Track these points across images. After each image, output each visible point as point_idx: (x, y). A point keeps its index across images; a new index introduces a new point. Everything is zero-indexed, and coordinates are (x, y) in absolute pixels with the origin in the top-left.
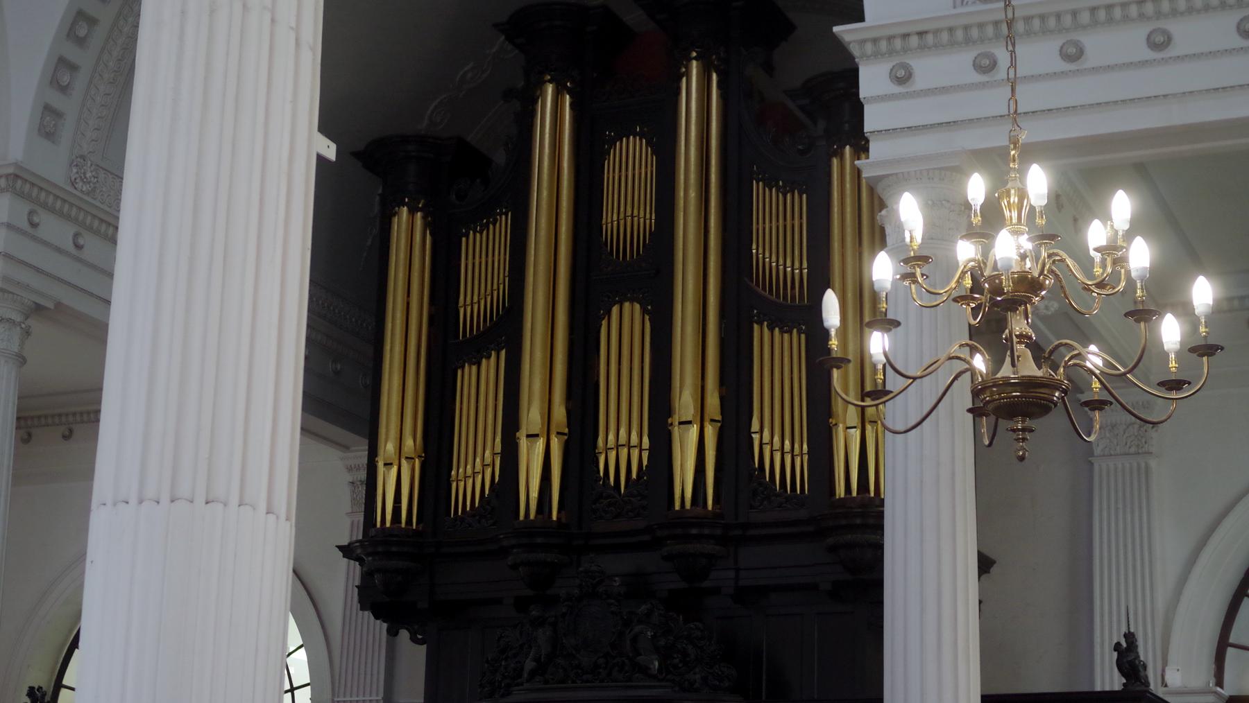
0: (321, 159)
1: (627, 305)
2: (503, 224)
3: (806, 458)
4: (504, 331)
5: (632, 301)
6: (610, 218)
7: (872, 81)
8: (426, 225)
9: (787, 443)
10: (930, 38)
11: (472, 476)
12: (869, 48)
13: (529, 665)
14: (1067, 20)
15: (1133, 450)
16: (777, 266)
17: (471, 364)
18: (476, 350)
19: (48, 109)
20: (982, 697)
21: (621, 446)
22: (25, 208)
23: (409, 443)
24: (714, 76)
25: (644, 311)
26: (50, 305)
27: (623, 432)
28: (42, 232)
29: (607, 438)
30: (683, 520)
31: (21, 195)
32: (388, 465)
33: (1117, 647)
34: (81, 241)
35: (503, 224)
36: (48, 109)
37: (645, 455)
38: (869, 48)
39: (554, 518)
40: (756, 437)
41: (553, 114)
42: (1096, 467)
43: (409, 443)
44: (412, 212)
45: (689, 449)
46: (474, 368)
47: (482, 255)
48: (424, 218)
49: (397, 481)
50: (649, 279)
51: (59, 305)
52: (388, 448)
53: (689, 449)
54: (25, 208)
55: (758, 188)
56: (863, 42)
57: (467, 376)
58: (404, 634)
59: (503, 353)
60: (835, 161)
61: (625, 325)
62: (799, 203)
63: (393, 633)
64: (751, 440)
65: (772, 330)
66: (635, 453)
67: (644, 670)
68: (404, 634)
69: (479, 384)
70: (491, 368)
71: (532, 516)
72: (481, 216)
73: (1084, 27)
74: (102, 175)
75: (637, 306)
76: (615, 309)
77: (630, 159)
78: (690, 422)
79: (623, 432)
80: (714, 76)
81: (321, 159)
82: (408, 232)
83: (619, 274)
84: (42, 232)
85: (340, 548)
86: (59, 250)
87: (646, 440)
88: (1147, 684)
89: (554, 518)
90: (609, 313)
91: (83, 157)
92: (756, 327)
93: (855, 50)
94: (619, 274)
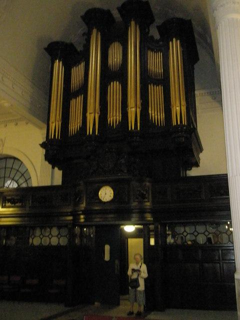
1: (115, 82)
2: (82, 65)
3: (139, 111)
6: (110, 62)
11: (74, 125)
16: (160, 114)
17: (74, 98)
18: (75, 95)
20: (235, 309)
21: (114, 117)
30: (132, 131)
32: (52, 123)
35: (82, 65)
37: (120, 118)
43: (58, 117)
45: (133, 111)
53: (133, 111)
57: (73, 102)
58: (56, 169)
60: (171, 43)
61: (115, 87)
62: (160, 54)
63: (53, 168)
68: (56, 169)
69: (76, 104)
71: (91, 133)
72: (77, 63)
75: (118, 82)
76: (112, 83)
82: (58, 67)
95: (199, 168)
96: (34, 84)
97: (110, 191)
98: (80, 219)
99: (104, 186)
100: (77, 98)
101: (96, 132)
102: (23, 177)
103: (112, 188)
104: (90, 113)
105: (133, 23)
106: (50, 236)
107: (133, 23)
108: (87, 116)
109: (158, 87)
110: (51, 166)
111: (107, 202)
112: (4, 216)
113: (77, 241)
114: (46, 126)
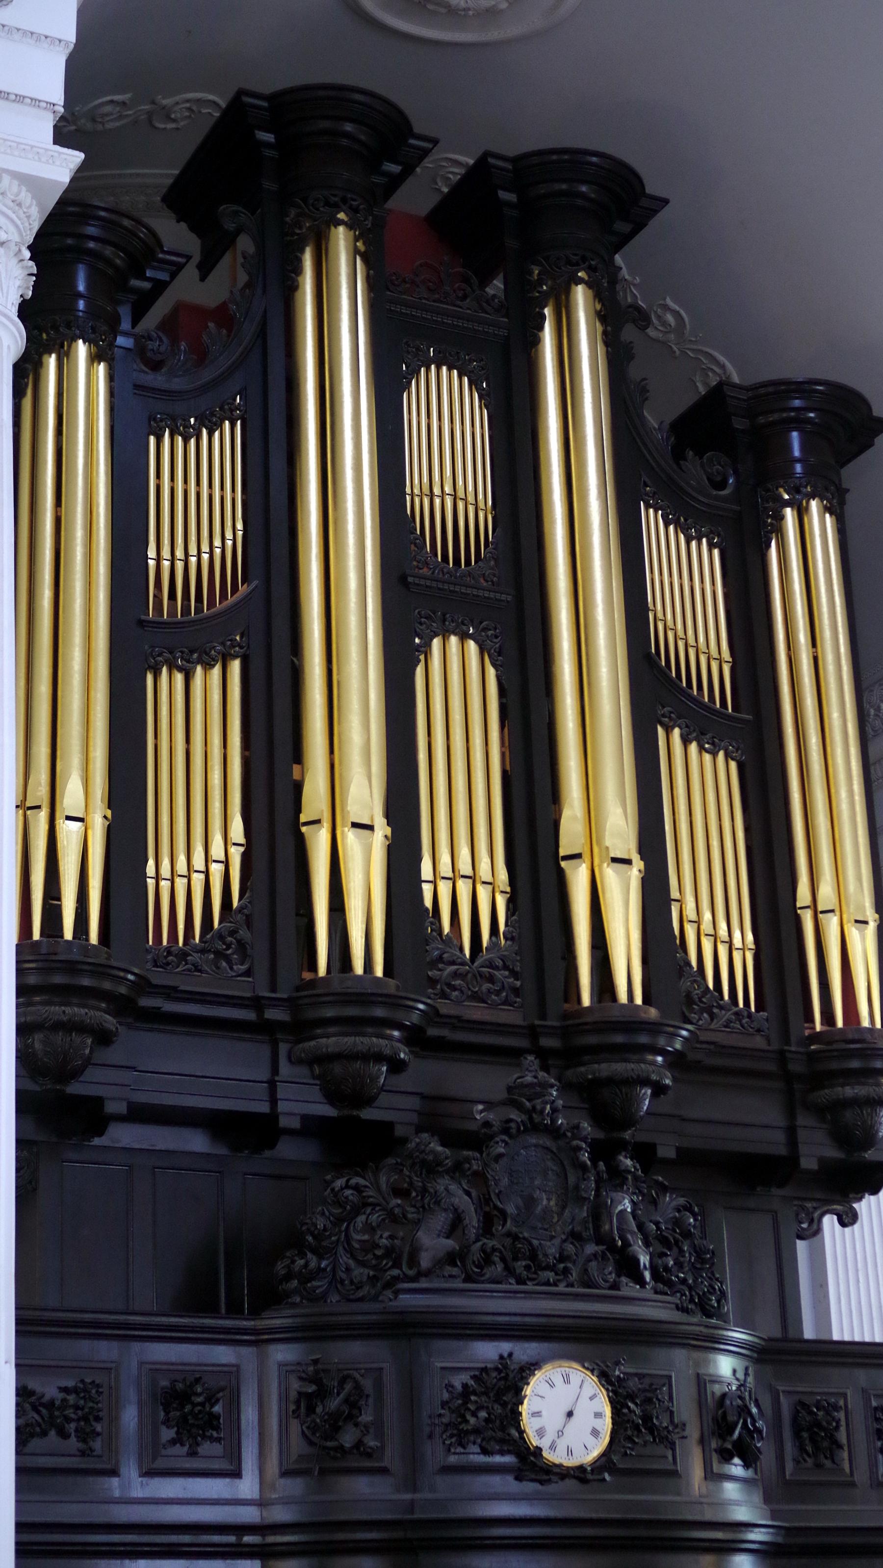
46: (179, 678)
57: (165, 688)
59: (235, 666)
65: (686, 742)
67: (629, 1267)
75: (472, 646)
97: (570, 1452)
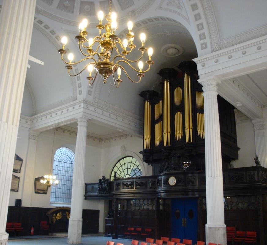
0: (28, 68)
1: (178, 112)
2: (161, 102)
3: (191, 130)
4: (161, 118)
5: (179, 112)
6: (176, 100)
7: (199, 68)
8: (150, 104)
9: (203, 131)
10: (208, 59)
11: (157, 141)
12: (198, 62)
13: (165, 168)
14: (229, 52)
15: (261, 129)
18: (157, 122)
19: (89, 91)
21: (178, 135)
22: (86, 105)
23: (148, 136)
24: (189, 76)
25: (181, 113)
26: (91, 119)
27: (179, 131)
28: (97, 111)
29: (177, 133)
31: (85, 103)
32: (145, 140)
33: (255, 159)
34: (95, 109)
35: (161, 102)
36: (89, 91)
37: (182, 135)
38: (198, 62)
39: (169, 145)
40: (198, 131)
41: (167, 86)
42: (255, 132)
43: (148, 136)
44: (147, 102)
47: (158, 107)
48: (149, 103)
49: (147, 141)
50: (181, 108)
51: (92, 119)
52: (145, 137)
54: (86, 105)
55: (197, 92)
56: (197, 61)
57: (156, 125)
60: (181, 138)
61: (178, 115)
64: (197, 131)
65: (200, 114)
66: (181, 135)
69: (158, 126)
70: (160, 124)
72: (157, 102)
73: (232, 53)
74: (99, 100)
75: (180, 113)
76: (177, 113)
77: (178, 90)
78: (187, 129)
79: (179, 131)
80: (189, 76)
81: (28, 68)
82: (147, 105)
83: (176, 108)
84: (97, 111)
85: (139, 152)
86: (100, 114)
87: (182, 133)
88: (260, 165)
89: (169, 145)
90: (176, 114)
91: (96, 97)
92: (197, 114)
93: (196, 62)
94: (176, 108)
95: (240, 149)
96: (111, 9)
98: (228, 196)
99: (172, 176)
100: (159, 123)
101: (190, 77)
102: (121, 165)
103: (175, 178)
104: (165, 133)
105: (186, 76)
106: (148, 204)
107: (186, 76)
108: (163, 136)
109: (199, 114)
110: (147, 164)
111: (173, 186)
112: (90, 198)
113: (161, 207)
114: (142, 136)
